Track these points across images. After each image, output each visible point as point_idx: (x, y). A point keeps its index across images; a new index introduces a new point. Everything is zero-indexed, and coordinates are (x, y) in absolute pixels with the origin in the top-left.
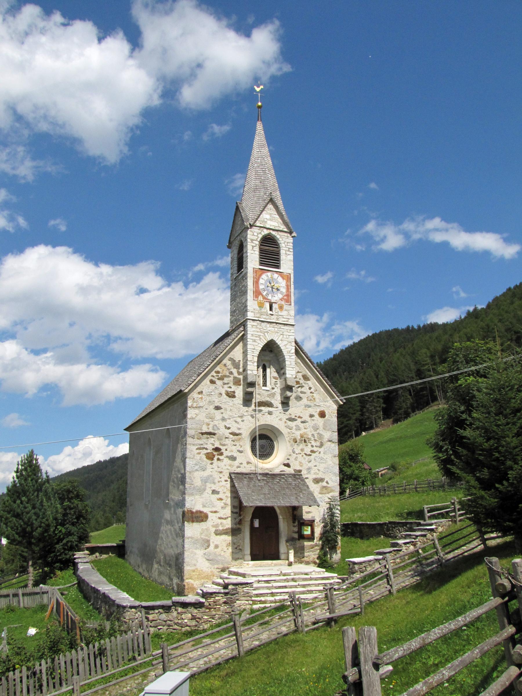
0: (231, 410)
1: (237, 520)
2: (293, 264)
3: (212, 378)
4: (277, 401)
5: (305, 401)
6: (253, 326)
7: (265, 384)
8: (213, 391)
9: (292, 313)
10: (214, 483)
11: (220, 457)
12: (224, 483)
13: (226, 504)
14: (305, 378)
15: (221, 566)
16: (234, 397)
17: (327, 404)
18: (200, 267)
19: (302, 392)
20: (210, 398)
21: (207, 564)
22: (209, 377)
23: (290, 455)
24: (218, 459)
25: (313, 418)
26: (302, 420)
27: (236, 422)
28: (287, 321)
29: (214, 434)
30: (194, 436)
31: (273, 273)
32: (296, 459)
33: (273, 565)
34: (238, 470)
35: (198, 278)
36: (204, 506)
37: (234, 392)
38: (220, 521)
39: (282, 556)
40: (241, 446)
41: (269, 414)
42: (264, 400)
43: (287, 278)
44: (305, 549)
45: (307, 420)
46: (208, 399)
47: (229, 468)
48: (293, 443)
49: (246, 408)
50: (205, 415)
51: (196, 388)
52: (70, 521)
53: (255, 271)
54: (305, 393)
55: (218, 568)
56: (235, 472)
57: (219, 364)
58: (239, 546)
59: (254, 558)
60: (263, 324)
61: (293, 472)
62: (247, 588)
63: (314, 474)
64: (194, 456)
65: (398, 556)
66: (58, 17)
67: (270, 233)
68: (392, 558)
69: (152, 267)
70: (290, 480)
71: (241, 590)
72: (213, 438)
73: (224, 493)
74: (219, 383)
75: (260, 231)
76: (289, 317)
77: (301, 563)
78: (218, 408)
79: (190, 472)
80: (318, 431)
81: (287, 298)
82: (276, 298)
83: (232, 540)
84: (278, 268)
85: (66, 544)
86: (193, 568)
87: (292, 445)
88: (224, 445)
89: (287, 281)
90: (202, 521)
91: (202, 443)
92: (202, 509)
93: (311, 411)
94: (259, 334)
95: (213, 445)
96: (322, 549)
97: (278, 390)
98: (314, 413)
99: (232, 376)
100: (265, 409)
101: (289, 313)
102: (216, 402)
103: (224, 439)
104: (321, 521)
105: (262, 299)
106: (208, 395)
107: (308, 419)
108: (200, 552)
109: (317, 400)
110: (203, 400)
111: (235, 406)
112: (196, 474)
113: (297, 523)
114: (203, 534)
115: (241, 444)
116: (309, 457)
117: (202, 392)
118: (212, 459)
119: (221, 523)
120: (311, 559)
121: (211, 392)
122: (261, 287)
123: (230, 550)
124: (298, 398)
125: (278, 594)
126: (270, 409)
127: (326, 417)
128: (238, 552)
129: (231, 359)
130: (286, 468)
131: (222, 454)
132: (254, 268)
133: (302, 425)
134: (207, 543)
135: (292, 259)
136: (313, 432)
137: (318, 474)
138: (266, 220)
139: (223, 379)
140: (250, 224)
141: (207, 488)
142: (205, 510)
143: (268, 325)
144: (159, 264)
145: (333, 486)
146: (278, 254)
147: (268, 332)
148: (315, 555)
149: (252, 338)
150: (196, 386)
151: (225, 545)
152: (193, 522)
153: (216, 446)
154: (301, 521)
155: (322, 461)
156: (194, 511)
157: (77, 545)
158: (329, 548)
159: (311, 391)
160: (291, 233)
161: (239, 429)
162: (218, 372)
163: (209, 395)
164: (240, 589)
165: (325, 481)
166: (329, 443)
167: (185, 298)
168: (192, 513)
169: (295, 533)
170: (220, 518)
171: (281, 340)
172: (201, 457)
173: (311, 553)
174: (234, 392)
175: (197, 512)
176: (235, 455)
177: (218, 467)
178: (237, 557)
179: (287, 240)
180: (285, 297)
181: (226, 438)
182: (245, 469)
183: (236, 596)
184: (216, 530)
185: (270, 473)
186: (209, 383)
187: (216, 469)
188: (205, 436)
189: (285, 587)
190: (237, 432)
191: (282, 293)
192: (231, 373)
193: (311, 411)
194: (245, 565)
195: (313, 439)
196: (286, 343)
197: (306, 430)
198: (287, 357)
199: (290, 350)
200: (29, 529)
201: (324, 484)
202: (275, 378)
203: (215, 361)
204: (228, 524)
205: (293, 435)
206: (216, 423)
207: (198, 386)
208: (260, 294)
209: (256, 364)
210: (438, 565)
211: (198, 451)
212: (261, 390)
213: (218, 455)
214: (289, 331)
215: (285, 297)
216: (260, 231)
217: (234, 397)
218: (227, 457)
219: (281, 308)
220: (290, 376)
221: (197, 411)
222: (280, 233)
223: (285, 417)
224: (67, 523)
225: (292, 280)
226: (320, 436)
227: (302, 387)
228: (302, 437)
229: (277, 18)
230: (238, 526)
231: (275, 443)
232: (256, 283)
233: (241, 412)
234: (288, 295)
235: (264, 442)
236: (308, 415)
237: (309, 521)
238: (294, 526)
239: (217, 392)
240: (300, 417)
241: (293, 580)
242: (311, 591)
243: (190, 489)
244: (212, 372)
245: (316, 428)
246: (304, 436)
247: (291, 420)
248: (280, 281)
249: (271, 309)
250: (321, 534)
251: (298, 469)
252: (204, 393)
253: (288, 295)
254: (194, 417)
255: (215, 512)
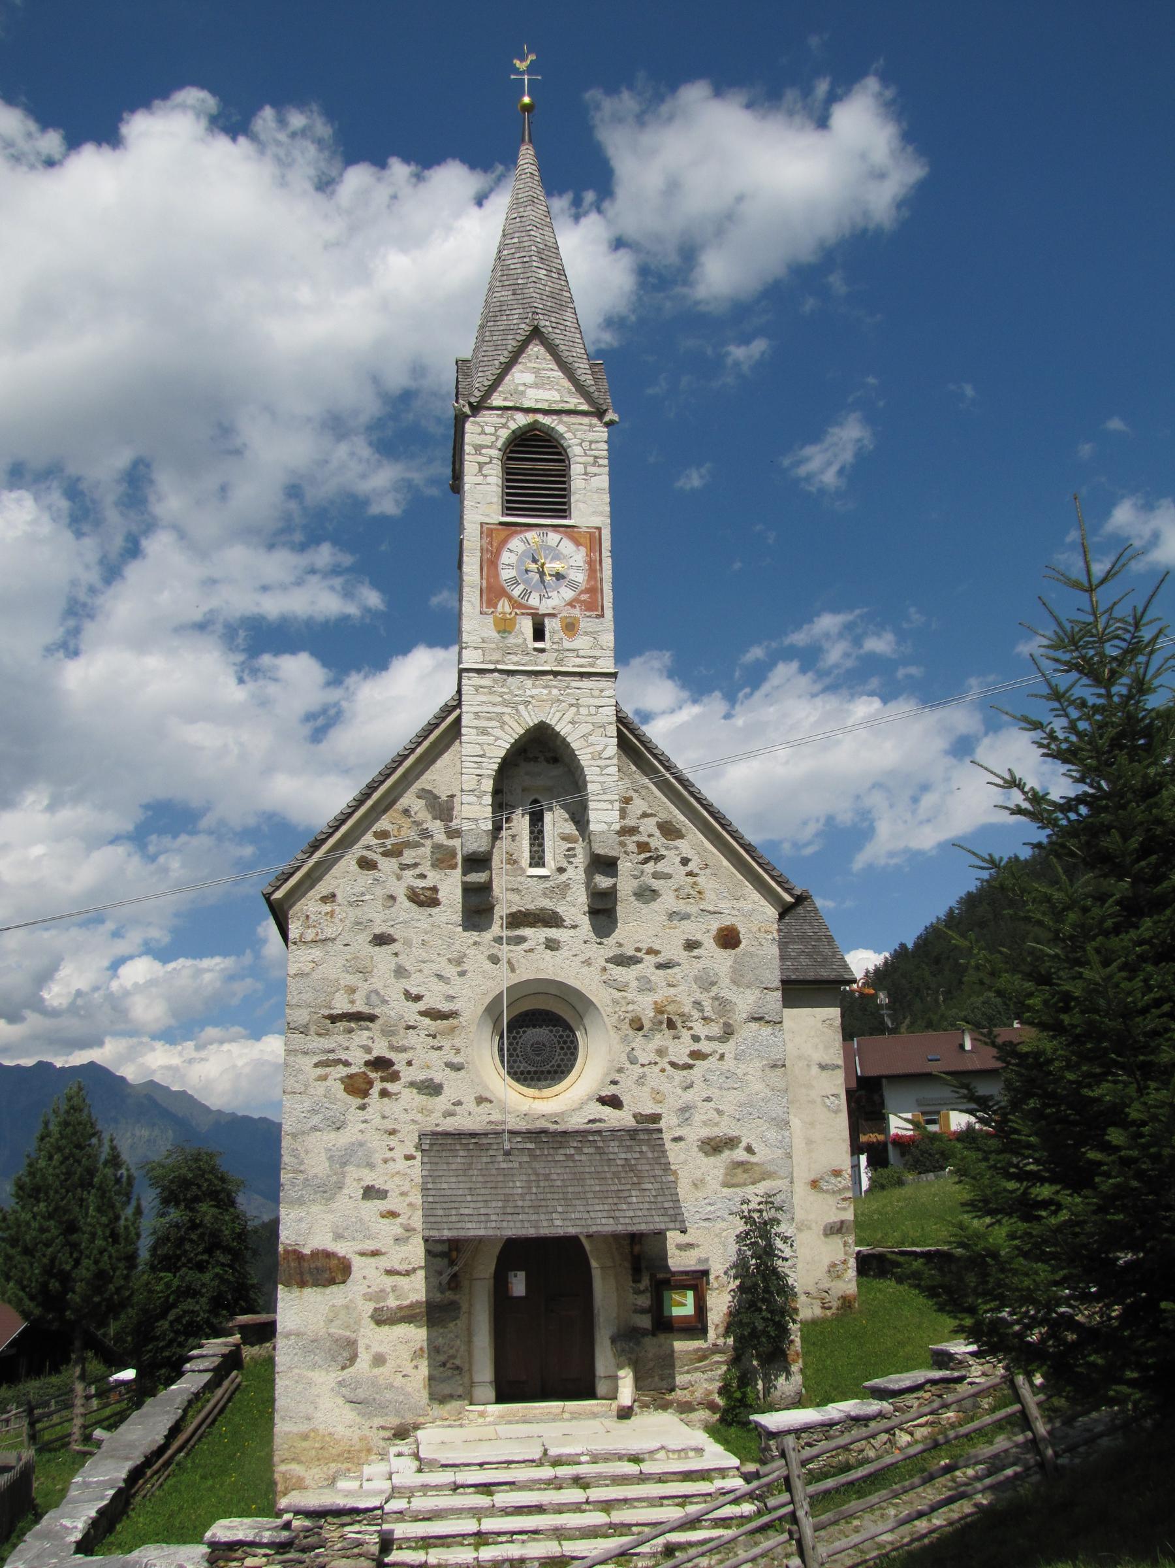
0: (424, 943)
1: (445, 1278)
2: (608, 500)
3: (365, 853)
4: (575, 907)
5: (668, 900)
6: (477, 688)
7: (537, 860)
8: (369, 890)
9: (608, 639)
10: (371, 1166)
11: (390, 1087)
12: (401, 1165)
13: (408, 1229)
14: (669, 831)
15: (394, 1421)
16: (434, 903)
17: (746, 905)
18: (756, 653)
19: (657, 876)
20: (358, 911)
21: (349, 1414)
22: (357, 851)
23: (620, 1070)
24: (384, 1093)
25: (696, 952)
26: (661, 959)
27: (439, 977)
28: (592, 666)
29: (372, 1018)
30: (306, 1026)
31: (545, 530)
32: (641, 1080)
33: (566, 1415)
34: (450, 1125)
35: (756, 677)
36: (338, 1237)
37: (435, 889)
38: (390, 1281)
39: (601, 1388)
40: (458, 1051)
41: (548, 947)
42: (531, 907)
43: (592, 541)
44: (678, 1363)
45: (676, 959)
46: (353, 914)
47: (419, 1117)
48: (631, 1032)
49: (474, 936)
50: (341, 962)
51: (312, 887)
52: (190, 1260)
53: (487, 531)
54: (668, 876)
55: (383, 1428)
56: (439, 1129)
57: (385, 811)
58: (453, 1357)
59: (508, 1391)
60: (511, 679)
61: (631, 1122)
62: (356, 1527)
63: (705, 1123)
64: (306, 1086)
65: (949, 1398)
66: (399, 170)
67: (536, 422)
68: (927, 1409)
69: (656, 664)
70: (614, 1147)
71: (336, 1534)
72: (368, 1029)
73: (403, 1194)
74: (387, 865)
75: (503, 421)
76: (598, 653)
77: (665, 1407)
78: (382, 940)
79: (294, 1136)
80: (715, 989)
81: (590, 601)
82: (556, 600)
83: (430, 1340)
84: (565, 517)
85: (178, 1319)
86: (304, 1428)
87: (625, 1039)
88: (403, 1049)
89: (591, 549)
90: (332, 1282)
91: (332, 1046)
92: (332, 1247)
93: (689, 929)
94: (498, 709)
95: (368, 1050)
96: (736, 1360)
97: (576, 874)
98: (698, 937)
99: (428, 843)
100: (535, 935)
101: (596, 641)
102: (378, 921)
103: (402, 1031)
104: (732, 1272)
105: (508, 609)
106: (350, 904)
107: (681, 955)
108: (325, 1379)
109: (710, 895)
110: (336, 920)
111: (437, 930)
112: (313, 1139)
113: (645, 1282)
114: (337, 1322)
115: (457, 1045)
116: (685, 1073)
117: (334, 896)
118: (365, 1094)
119: (394, 1289)
120: (699, 1394)
121: (363, 894)
122: (506, 574)
123: (424, 1370)
124: (647, 894)
125: (503, 1539)
126: (552, 933)
127: (742, 946)
128: (449, 1378)
129: (425, 794)
130: (608, 1110)
131: (395, 1077)
132: (482, 524)
133: (658, 976)
134: (346, 1351)
135: (606, 485)
136: (698, 996)
137: (717, 1124)
138: (521, 388)
139: (400, 854)
140: (470, 404)
141: (348, 1180)
142: (342, 1249)
143: (529, 682)
144: (667, 657)
145: (772, 1161)
146: (563, 475)
147: (526, 703)
148: (712, 1380)
149: (476, 723)
150: (312, 879)
151: (407, 1355)
152: (302, 1284)
153: (375, 1053)
154: (661, 1276)
155: (730, 1083)
156: (307, 1251)
157: (207, 1321)
158: (759, 1357)
159: (688, 869)
160: (600, 414)
161: (451, 998)
162: (384, 835)
163: (358, 903)
164: (330, 1531)
165: (743, 1144)
166: (754, 1026)
167: (740, 722)
168: (299, 1256)
169: (643, 1311)
170: (390, 1272)
171: (572, 722)
172: (328, 1089)
173: (698, 1374)
174: (435, 889)
175: (315, 1254)
176: (438, 1078)
177: (384, 1117)
178: (447, 1391)
179: (591, 436)
180: (584, 597)
181: (409, 1027)
182: (471, 1119)
183: (318, 1556)
184: (376, 1309)
185: (553, 1127)
186: (354, 867)
187: (377, 1121)
188: (342, 1025)
189: (539, 1509)
190: (445, 1007)
191: (572, 585)
192: (426, 834)
193: (689, 929)
194: (471, 1416)
195: (696, 1015)
196: (585, 729)
197: (672, 991)
198: (591, 772)
199: (600, 748)
200: (54, 1285)
201: (740, 1154)
202: (566, 838)
203: (370, 803)
204: (415, 1289)
205: (630, 1007)
206: (376, 983)
207: (319, 879)
208: (503, 593)
209: (488, 799)
210: (1027, 1469)
211: (320, 1071)
212: (522, 879)
213: (383, 1079)
214: (596, 693)
215: (584, 597)
216: (503, 421)
217: (434, 903)
218: (412, 1084)
219: (570, 627)
220: (604, 827)
221: (316, 953)
222: (566, 418)
223: (601, 952)
224: (184, 1265)
225: (607, 544)
226: (723, 1004)
227: (658, 858)
228: (662, 1012)
229: (876, 74)
230: (449, 1295)
231: (578, 1034)
232: (490, 563)
233: (457, 947)
234: (594, 590)
235: (539, 1033)
236: (680, 942)
237: (686, 1273)
238: (638, 1292)
239: (380, 892)
240: (650, 951)
241: (579, 1482)
242: (623, 1525)
243: (293, 1185)
244: (363, 833)
245: (707, 982)
246: (669, 1008)
247: (622, 961)
248: (565, 552)
249: (539, 634)
250: (730, 1314)
251: (648, 1111)
252: (339, 898)
253: (594, 590)
254: (307, 970)
255: (375, 1254)
